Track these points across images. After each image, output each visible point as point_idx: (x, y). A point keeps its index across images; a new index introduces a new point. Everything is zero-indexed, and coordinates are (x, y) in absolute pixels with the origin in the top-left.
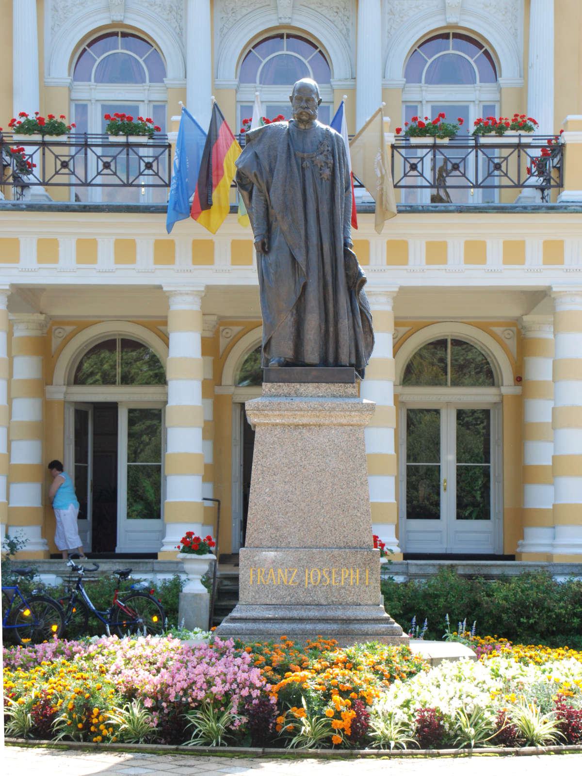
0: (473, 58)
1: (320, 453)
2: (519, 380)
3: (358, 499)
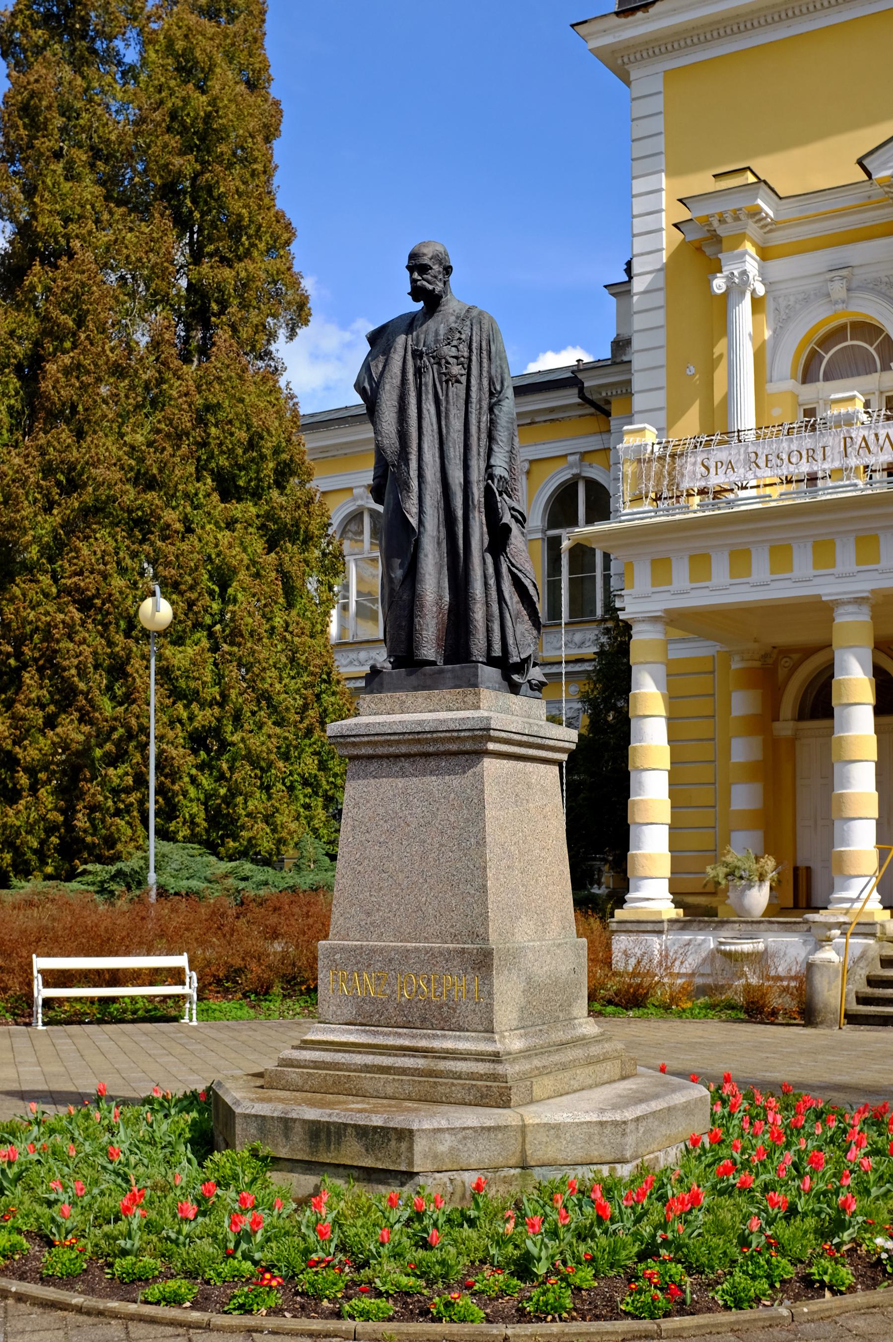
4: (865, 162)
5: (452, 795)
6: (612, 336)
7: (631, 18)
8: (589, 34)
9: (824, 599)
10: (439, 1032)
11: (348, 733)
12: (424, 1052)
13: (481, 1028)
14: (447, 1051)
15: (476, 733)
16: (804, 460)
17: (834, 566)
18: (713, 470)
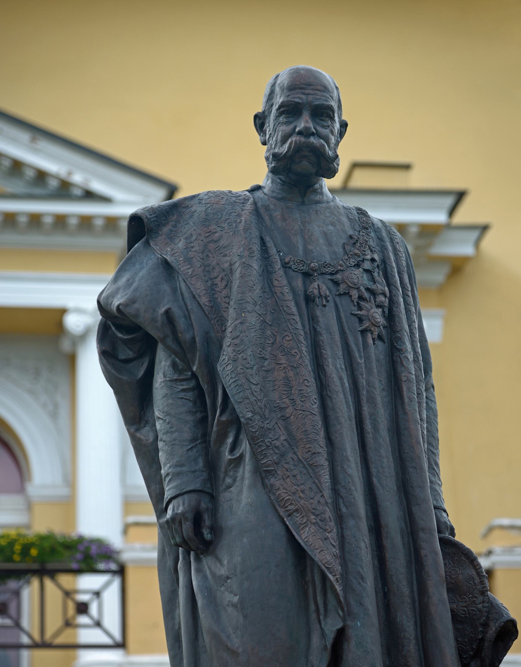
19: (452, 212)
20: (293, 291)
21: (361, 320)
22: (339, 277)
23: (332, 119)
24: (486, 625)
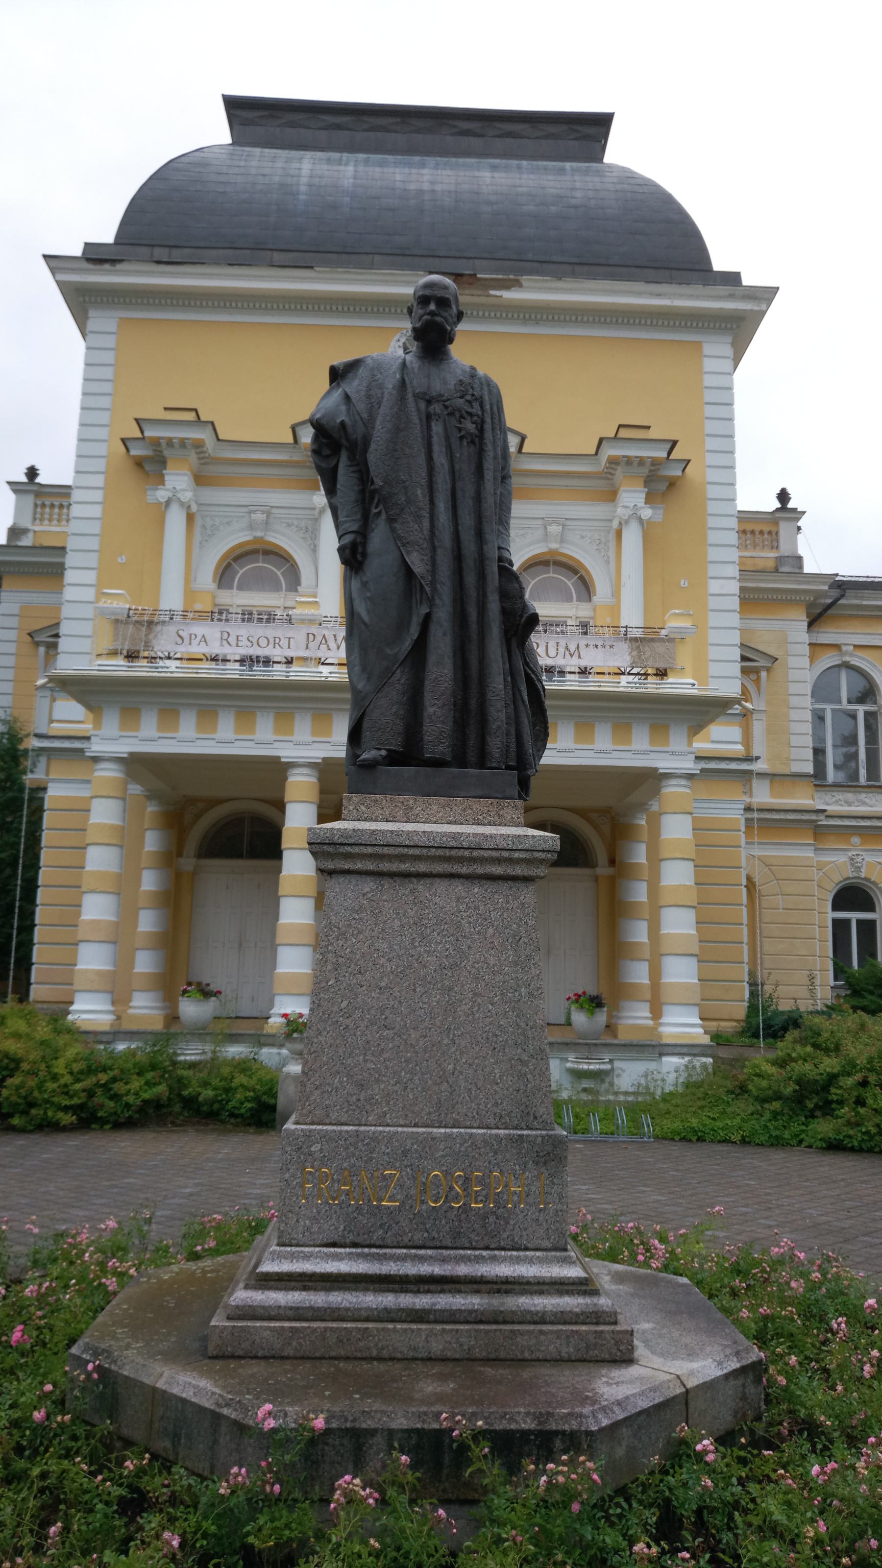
0: (570, 583)
1: (451, 931)
2: (612, 862)
3: (523, 1024)
4: (297, 429)
5: (491, 930)
6: (9, 523)
7: (98, 267)
8: (59, 269)
9: (283, 760)
10: (484, 1253)
11: (341, 840)
12: (476, 1284)
13: (546, 1244)
14: (569, 1293)
15: (537, 855)
16: (271, 645)
17: (292, 734)
18: (187, 641)
19: (669, 453)
20: (418, 410)
21: (460, 430)
22: (447, 403)
23: (450, 306)
24: (521, 616)
